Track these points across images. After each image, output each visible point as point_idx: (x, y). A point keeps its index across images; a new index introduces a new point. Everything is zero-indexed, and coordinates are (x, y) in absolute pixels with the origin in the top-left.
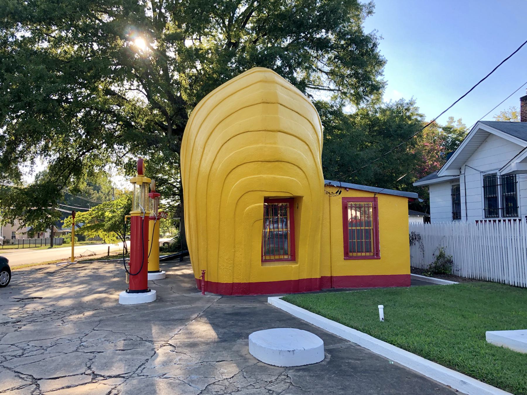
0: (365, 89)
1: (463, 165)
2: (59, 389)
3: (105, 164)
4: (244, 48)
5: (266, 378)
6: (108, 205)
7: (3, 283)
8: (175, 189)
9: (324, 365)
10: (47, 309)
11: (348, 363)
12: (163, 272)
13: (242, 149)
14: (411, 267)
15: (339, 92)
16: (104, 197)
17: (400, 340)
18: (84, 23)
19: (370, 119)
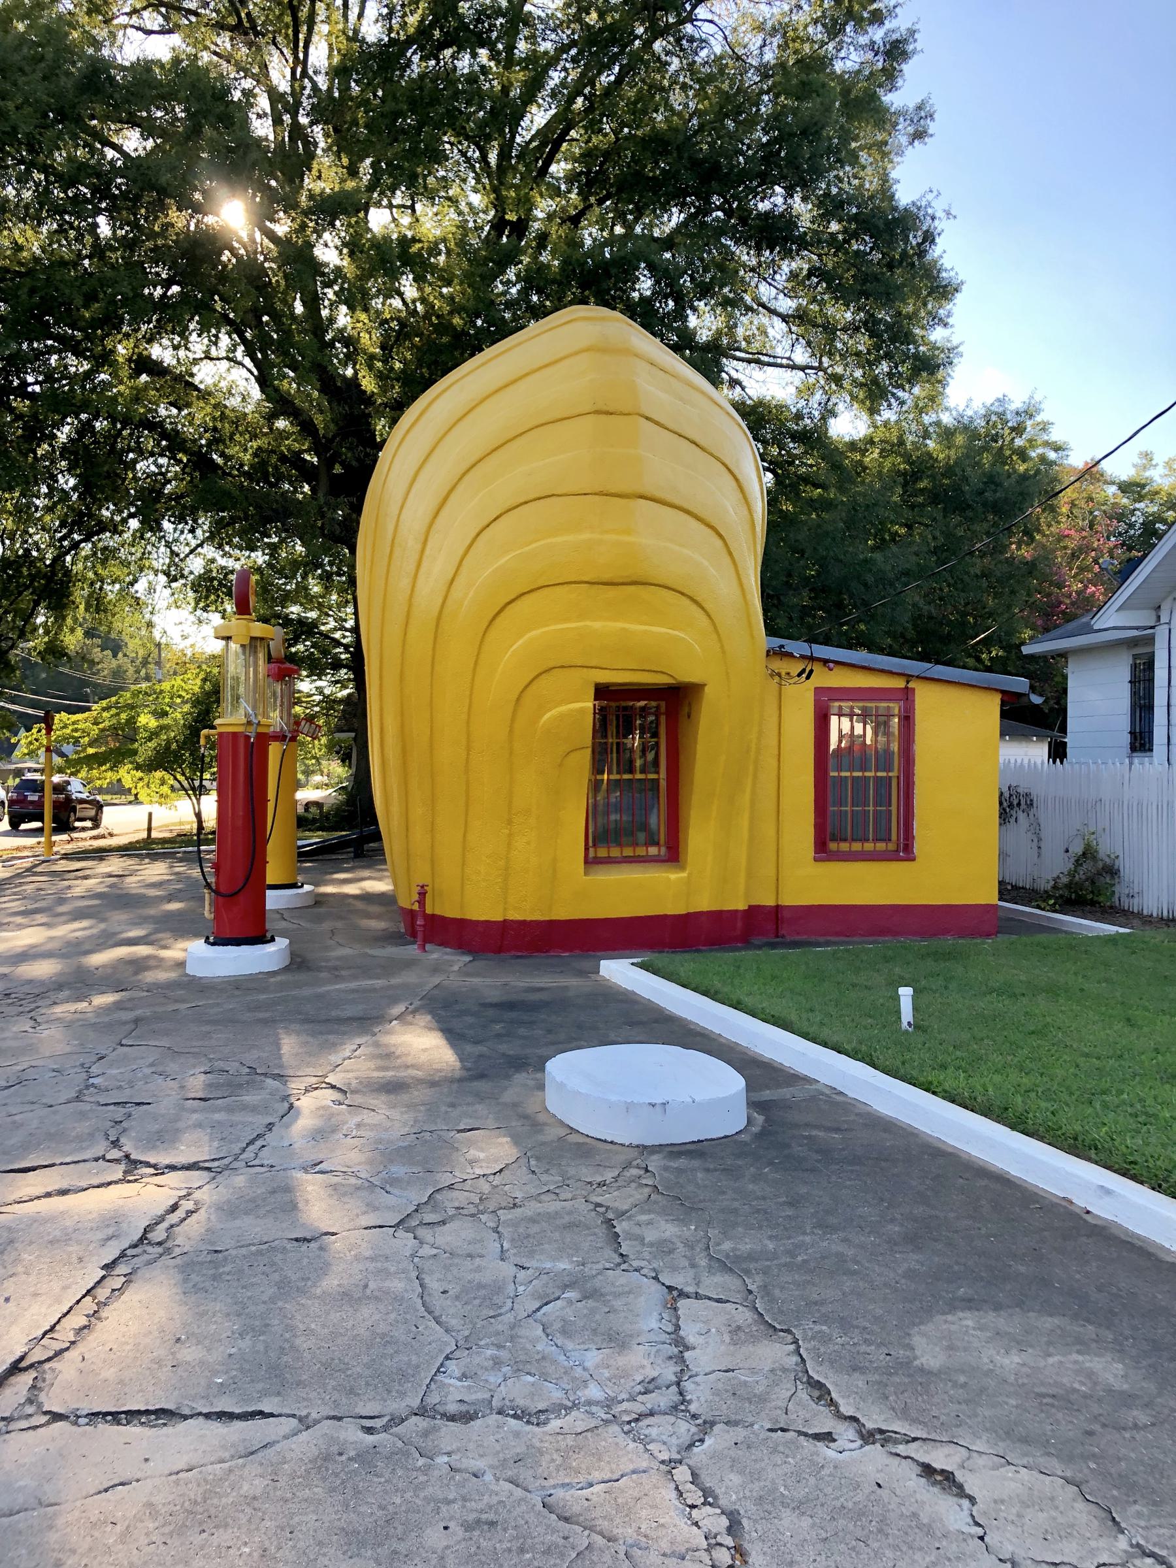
0: (896, 368)
1: (1164, 599)
2: (38, 1198)
3: (134, 575)
4: (543, 239)
5: (588, 1174)
6: (146, 693)
9: (746, 1144)
11: (809, 1137)
12: (307, 888)
13: (534, 545)
14: (1000, 883)
15: (821, 373)
16: (131, 670)
17: (953, 1080)
18: (71, 159)
19: (907, 458)
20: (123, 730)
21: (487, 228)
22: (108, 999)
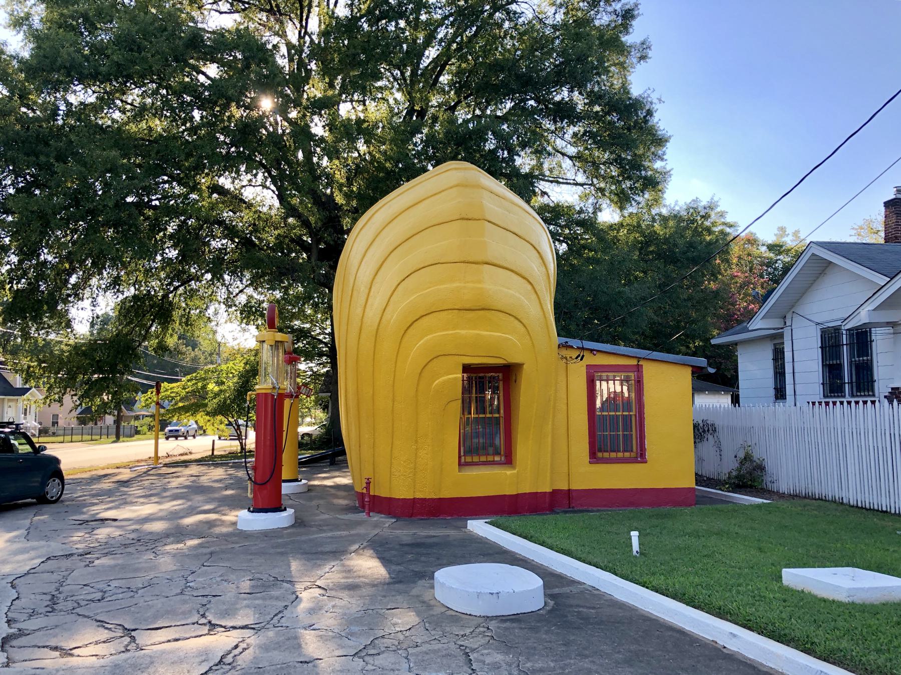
2: (164, 642)
4: (435, 119)
6: (213, 371)
7: (52, 497)
8: (321, 346)
9: (542, 615)
10: (128, 536)
11: (578, 612)
12: (304, 481)
14: (696, 474)
16: (203, 358)
17: (659, 581)
19: (643, 234)
20: (199, 393)
21: (405, 112)
22: (195, 542)
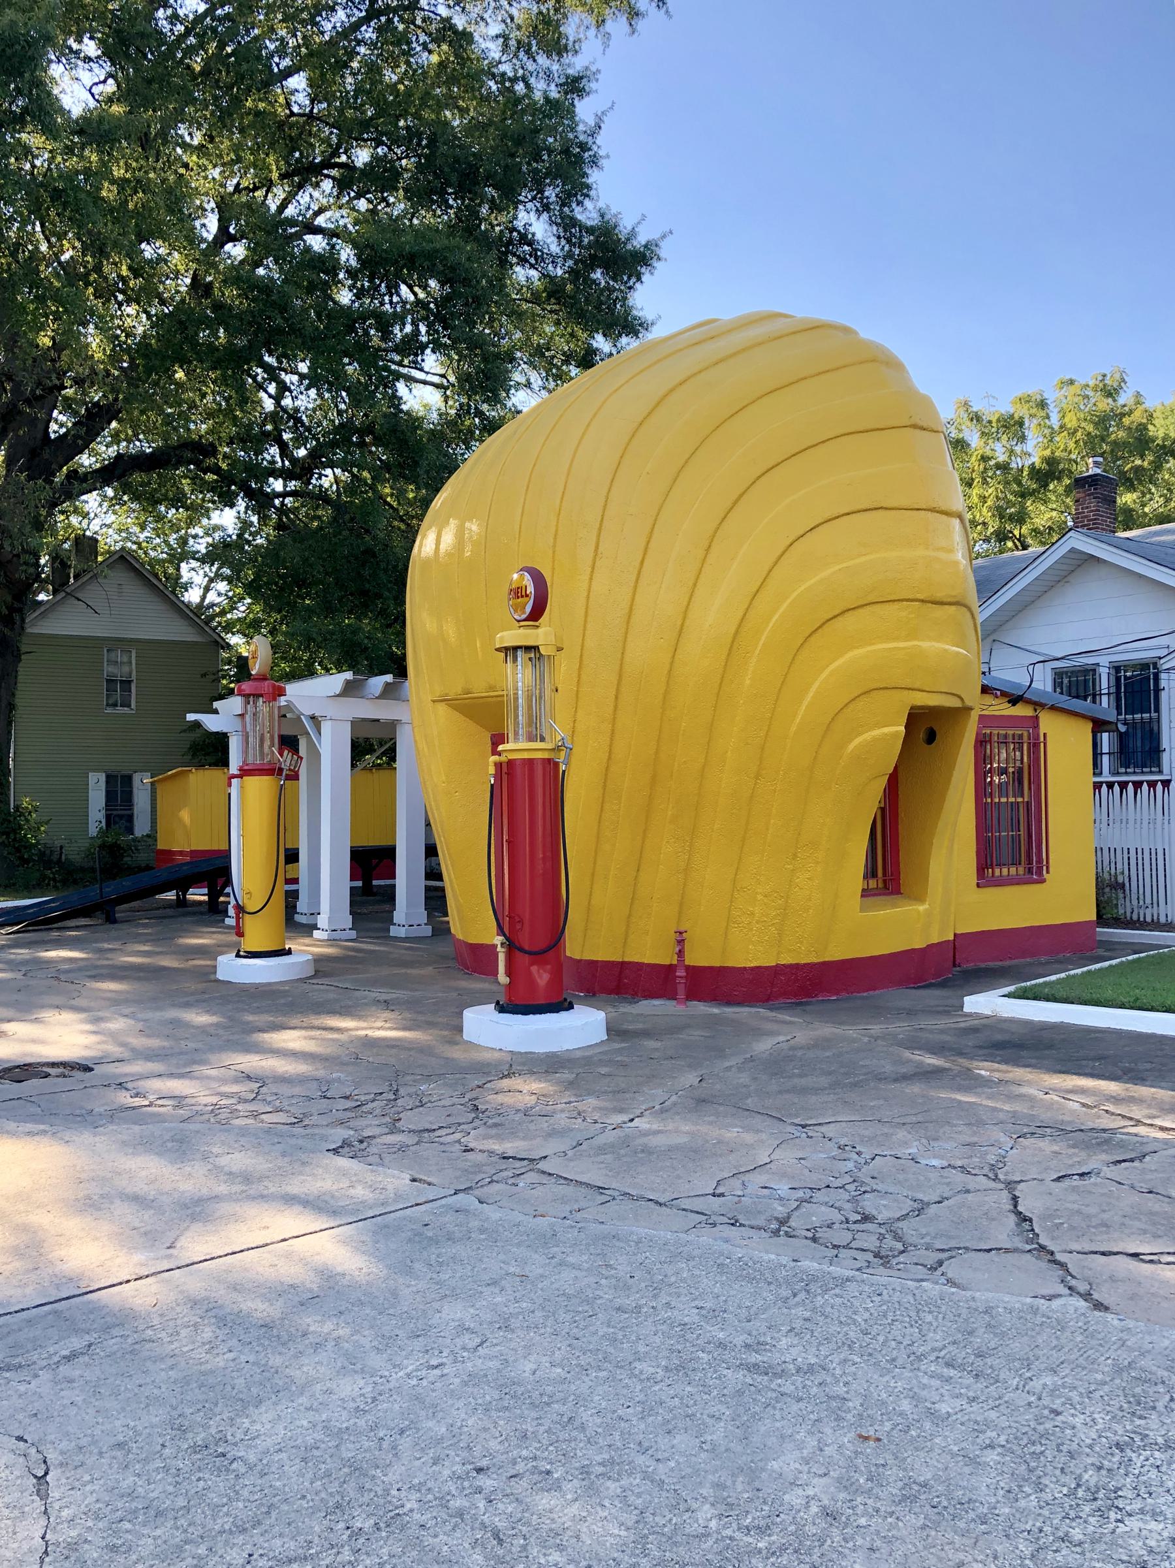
13: (863, 559)
